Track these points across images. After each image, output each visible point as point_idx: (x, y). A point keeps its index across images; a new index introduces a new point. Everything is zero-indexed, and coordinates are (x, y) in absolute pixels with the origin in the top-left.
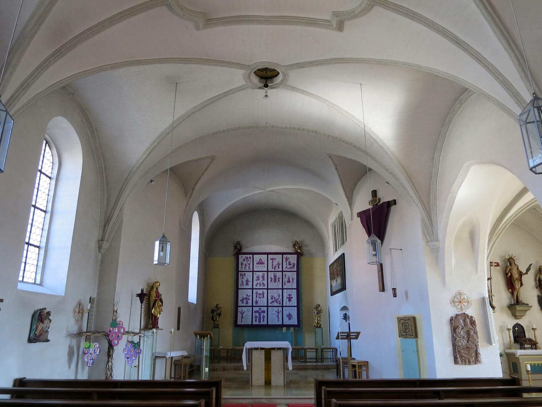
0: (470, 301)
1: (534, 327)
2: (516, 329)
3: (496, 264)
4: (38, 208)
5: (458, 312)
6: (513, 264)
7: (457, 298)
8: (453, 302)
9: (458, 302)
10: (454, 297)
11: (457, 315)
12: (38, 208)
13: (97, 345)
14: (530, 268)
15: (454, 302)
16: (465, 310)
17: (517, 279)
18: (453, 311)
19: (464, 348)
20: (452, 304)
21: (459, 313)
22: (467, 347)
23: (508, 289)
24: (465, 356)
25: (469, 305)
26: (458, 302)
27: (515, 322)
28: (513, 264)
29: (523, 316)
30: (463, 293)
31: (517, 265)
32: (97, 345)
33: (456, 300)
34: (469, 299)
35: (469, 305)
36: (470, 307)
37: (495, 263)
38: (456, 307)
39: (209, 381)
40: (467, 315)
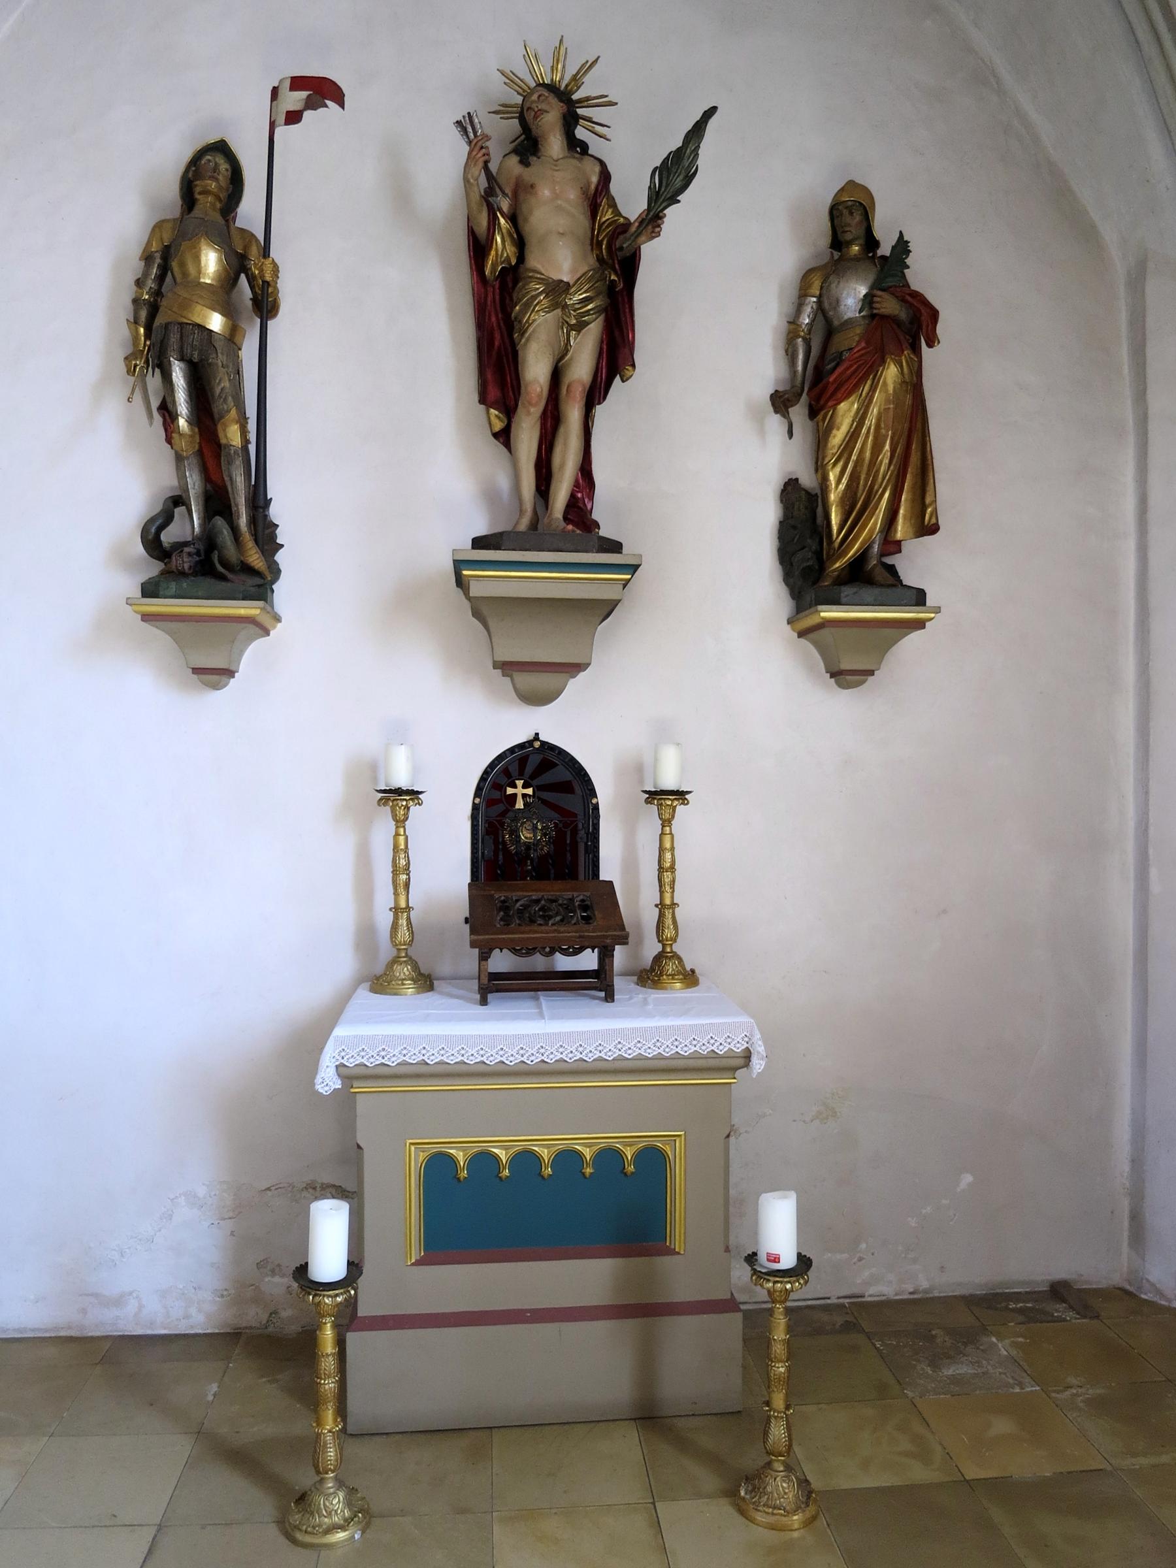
1: (669, 781)
6: (555, 145)
17: (558, 290)
28: (555, 145)
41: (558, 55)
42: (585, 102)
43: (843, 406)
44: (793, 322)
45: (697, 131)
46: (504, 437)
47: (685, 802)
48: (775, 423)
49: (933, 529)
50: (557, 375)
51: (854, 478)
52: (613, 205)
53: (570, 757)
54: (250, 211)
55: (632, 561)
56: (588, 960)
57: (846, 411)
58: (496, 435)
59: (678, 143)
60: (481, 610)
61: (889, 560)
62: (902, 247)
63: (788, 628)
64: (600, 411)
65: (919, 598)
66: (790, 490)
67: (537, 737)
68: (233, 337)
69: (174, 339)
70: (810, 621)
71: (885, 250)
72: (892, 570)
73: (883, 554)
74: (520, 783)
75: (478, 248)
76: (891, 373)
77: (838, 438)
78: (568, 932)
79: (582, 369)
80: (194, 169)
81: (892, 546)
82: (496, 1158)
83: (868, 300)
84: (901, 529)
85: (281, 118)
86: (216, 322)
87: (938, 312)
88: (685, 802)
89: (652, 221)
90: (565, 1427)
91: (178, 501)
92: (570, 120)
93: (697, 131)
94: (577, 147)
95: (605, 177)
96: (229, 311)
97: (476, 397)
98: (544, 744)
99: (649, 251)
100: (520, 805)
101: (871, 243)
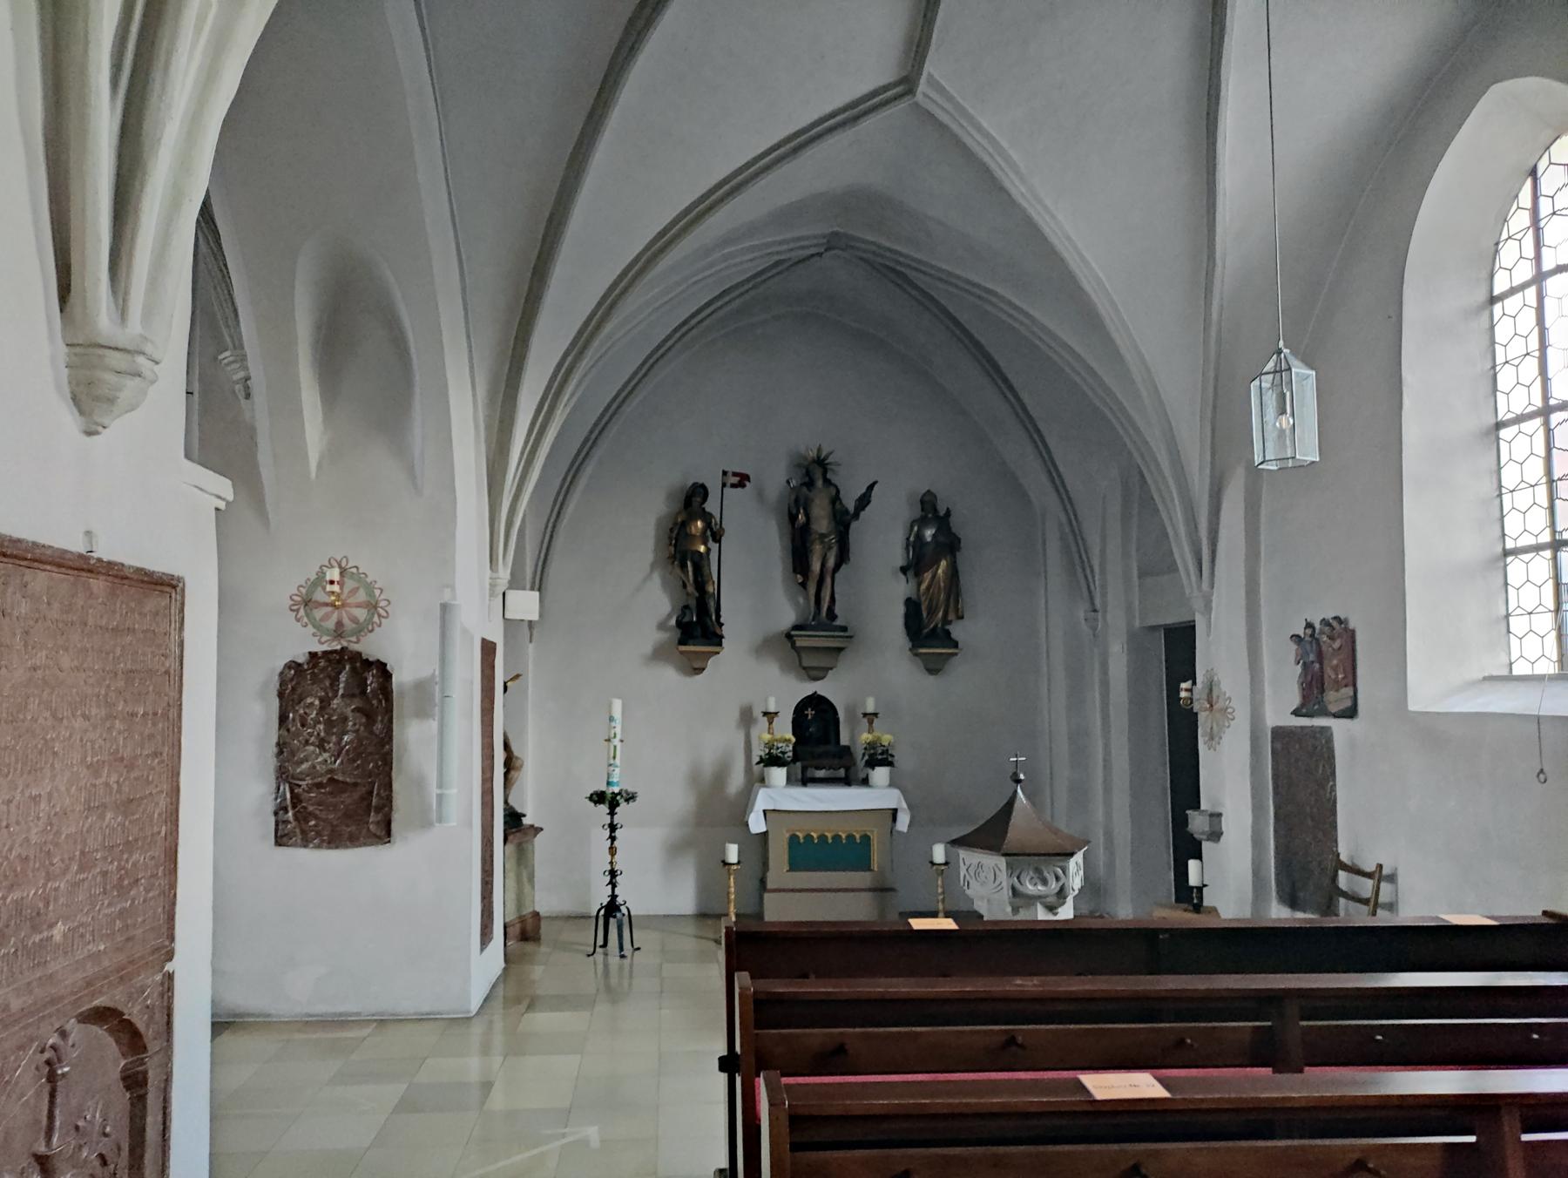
0: (383, 604)
1: (772, 709)
2: (810, 713)
3: (735, 480)
4: (1546, 395)
5: (323, 644)
6: (820, 483)
7: (354, 591)
8: (306, 605)
9: (326, 605)
10: (360, 580)
11: (313, 655)
12: (1546, 395)
13: (875, 832)
14: (870, 496)
15: (307, 602)
16: (354, 639)
17: (823, 536)
18: (301, 643)
19: (319, 785)
20: (298, 611)
21: (319, 648)
22: (332, 780)
23: (795, 571)
24: (323, 815)
25: (376, 616)
26: (326, 605)
27: (808, 688)
28: (820, 483)
29: (831, 669)
30: (354, 570)
31: (836, 487)
32: (875, 832)
33: (319, 596)
34: (377, 592)
35: (376, 616)
36: (380, 626)
37: (735, 474)
38: (314, 626)
39: (1011, 978)
40: (357, 656)
41: (819, 450)
42: (827, 464)
43: (926, 575)
44: (908, 539)
45: (871, 487)
46: (804, 585)
47: (877, 717)
48: (902, 577)
49: (962, 618)
50: (823, 565)
51: (931, 600)
52: (841, 503)
53: (171, 663)
54: (711, 506)
55: (851, 634)
56: (842, 773)
57: (928, 576)
58: (800, 584)
59: (864, 490)
60: (798, 650)
61: (947, 627)
62: (948, 513)
63: (909, 653)
64: (837, 575)
65: (956, 645)
66: (908, 602)
67: (816, 692)
68: (708, 550)
69: (689, 556)
70: (915, 651)
71: (942, 513)
72: (948, 633)
73: (943, 625)
74: (809, 709)
75: (793, 518)
76: (943, 563)
77: (924, 586)
78: (836, 761)
79: (831, 562)
80: (1195, 901)
81: (946, 621)
82: (812, 837)
83: (934, 536)
84: (951, 616)
85: (728, 485)
86: (702, 549)
87: (959, 540)
88: (877, 717)
89: (856, 515)
90: (1069, 489)
91: (686, 607)
92: (825, 472)
93: (871, 487)
94: (827, 482)
95: (838, 492)
96: (705, 543)
97: (791, 570)
98: (819, 695)
99: (854, 525)
100: (810, 717)
101: (935, 510)
